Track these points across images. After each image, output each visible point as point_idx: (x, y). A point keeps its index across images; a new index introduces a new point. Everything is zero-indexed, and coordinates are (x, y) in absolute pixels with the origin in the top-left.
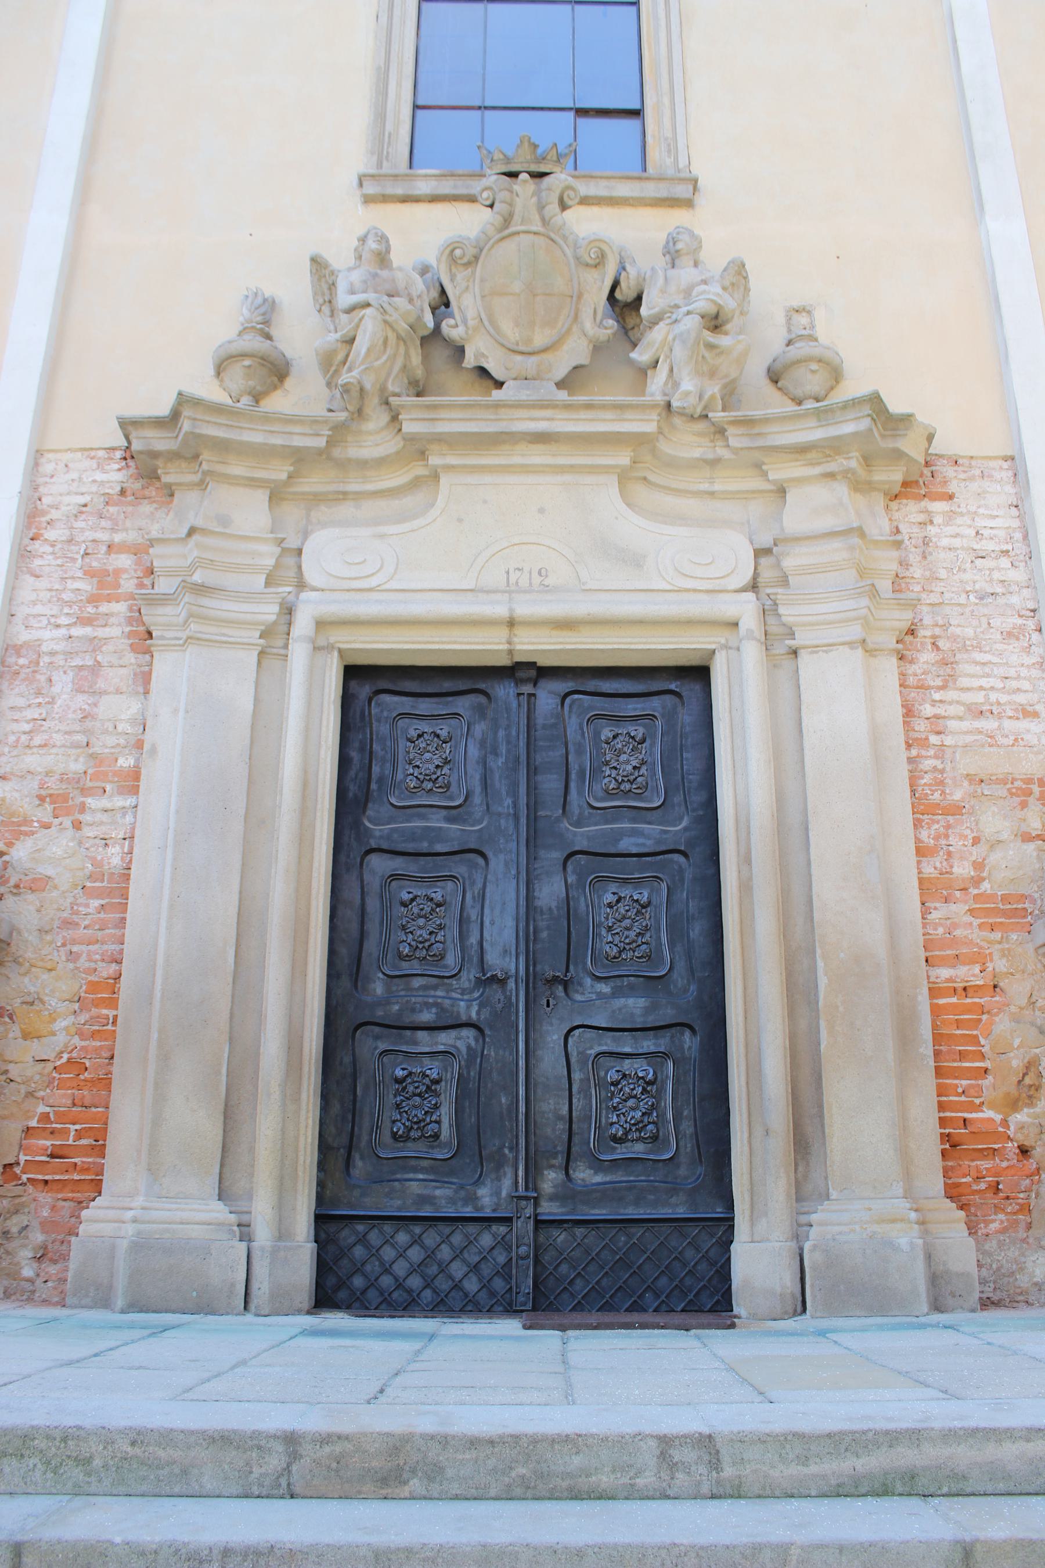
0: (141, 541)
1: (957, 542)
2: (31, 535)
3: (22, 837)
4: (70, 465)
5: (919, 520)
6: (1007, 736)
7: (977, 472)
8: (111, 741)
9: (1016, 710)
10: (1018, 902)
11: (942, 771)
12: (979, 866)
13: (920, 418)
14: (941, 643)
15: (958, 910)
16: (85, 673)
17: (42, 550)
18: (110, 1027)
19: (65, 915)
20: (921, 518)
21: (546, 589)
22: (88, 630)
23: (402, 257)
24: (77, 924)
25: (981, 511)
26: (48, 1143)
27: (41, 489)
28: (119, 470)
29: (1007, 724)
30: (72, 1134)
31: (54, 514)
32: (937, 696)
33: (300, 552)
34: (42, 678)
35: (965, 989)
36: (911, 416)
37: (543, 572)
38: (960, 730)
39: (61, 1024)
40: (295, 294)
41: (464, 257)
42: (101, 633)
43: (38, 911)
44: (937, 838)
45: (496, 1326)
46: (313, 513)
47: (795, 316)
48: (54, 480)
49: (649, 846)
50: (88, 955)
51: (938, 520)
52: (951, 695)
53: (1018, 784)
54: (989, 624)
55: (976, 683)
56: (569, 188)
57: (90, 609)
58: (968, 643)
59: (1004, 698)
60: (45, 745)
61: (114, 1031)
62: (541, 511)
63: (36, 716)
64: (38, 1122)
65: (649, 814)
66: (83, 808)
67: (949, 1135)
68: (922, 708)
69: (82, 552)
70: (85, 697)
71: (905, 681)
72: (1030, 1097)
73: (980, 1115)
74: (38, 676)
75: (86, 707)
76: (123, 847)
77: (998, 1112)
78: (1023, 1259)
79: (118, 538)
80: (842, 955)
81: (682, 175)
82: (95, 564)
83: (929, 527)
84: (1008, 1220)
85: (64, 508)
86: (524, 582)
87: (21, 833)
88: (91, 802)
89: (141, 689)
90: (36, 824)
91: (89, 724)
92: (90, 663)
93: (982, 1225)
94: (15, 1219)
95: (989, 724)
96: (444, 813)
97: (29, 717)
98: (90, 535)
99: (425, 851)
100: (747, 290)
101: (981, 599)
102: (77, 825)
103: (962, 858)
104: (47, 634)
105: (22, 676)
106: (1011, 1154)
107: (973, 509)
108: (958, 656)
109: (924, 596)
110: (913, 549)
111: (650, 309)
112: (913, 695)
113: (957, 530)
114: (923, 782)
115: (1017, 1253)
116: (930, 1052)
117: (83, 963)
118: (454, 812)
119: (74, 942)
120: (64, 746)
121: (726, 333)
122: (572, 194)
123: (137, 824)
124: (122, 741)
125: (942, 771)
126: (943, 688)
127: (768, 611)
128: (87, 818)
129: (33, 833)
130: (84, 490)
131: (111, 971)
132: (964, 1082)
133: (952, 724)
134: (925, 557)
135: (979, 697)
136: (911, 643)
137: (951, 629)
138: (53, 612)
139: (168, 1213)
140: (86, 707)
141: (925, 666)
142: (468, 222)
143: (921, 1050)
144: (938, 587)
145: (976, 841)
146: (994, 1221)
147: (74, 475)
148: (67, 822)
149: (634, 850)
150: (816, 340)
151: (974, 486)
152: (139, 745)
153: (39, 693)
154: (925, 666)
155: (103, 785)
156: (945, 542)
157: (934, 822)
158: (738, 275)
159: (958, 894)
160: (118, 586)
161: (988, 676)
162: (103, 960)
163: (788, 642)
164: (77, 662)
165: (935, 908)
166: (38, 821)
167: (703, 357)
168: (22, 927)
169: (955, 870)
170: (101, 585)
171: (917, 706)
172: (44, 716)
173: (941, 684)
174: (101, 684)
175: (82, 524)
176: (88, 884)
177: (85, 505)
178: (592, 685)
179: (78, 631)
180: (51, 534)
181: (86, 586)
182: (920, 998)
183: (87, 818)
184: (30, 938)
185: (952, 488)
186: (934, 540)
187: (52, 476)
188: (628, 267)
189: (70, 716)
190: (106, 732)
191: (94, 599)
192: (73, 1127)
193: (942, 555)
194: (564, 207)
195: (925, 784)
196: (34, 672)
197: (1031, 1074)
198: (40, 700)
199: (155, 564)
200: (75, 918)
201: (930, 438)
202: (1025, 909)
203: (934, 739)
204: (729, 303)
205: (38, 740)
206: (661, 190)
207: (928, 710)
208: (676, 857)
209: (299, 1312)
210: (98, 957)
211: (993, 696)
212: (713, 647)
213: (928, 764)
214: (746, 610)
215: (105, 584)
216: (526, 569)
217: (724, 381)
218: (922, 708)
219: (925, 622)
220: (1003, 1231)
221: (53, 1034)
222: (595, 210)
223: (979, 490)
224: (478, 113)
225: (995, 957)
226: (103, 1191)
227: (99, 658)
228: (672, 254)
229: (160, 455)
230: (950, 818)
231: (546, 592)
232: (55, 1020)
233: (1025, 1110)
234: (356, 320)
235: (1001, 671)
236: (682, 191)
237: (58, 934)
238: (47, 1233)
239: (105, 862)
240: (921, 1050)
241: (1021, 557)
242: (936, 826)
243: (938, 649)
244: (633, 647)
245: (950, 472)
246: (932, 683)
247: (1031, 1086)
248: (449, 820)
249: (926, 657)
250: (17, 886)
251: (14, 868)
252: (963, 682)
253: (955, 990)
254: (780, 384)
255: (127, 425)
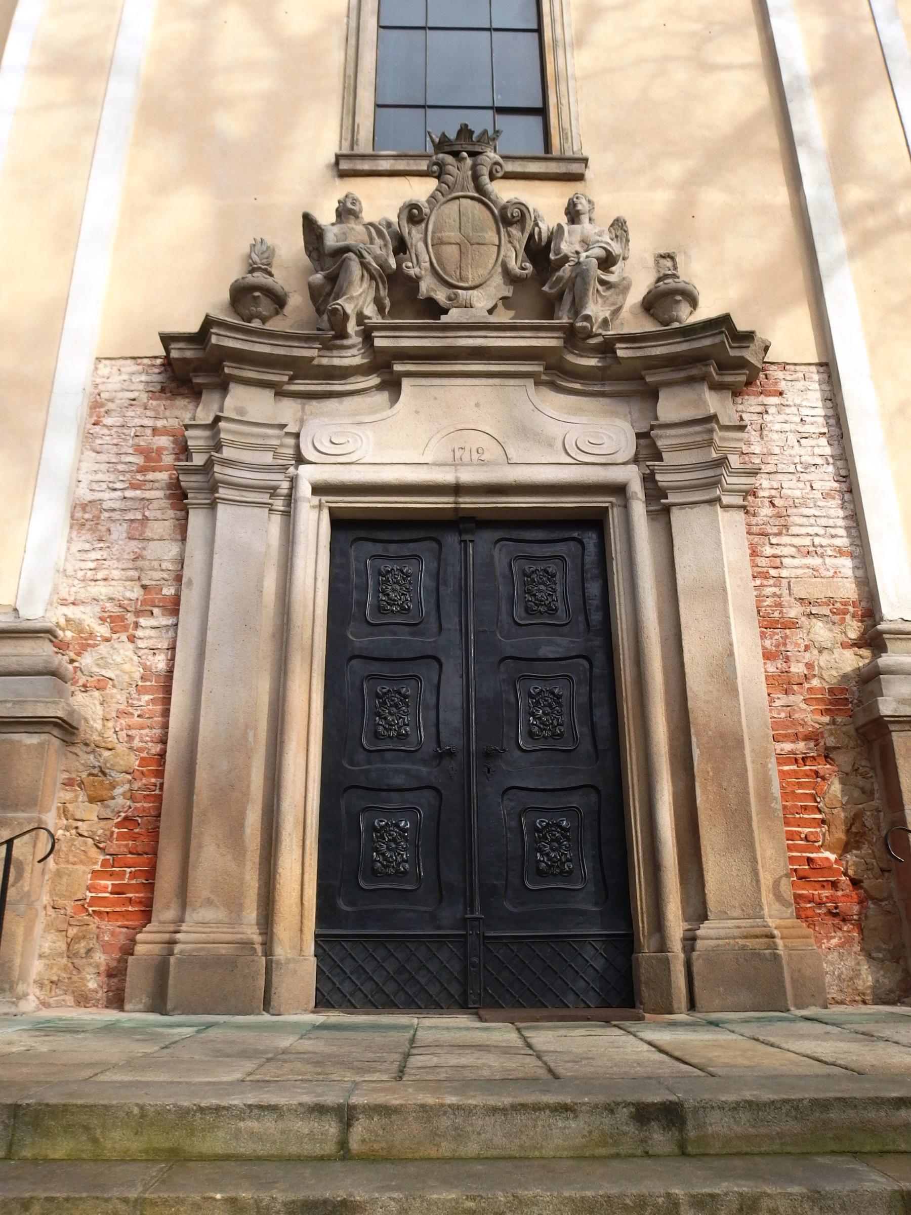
0: (177, 426)
1: (787, 427)
2: (93, 422)
3: (89, 649)
4: (122, 369)
5: (758, 411)
6: (828, 570)
7: (801, 375)
8: (157, 575)
9: (835, 550)
10: (841, 693)
11: (780, 597)
12: (809, 666)
13: (759, 334)
14: (777, 502)
15: (797, 699)
16: (135, 525)
17: (101, 432)
18: (157, 792)
19: (122, 707)
20: (760, 409)
21: (483, 463)
22: (138, 493)
23: (370, 214)
24: (132, 714)
25: (804, 403)
26: (109, 883)
27: (100, 387)
28: (159, 373)
29: (828, 560)
30: (127, 876)
31: (111, 406)
32: (774, 541)
33: (297, 436)
34: (103, 529)
35: (803, 759)
36: (753, 332)
37: (480, 451)
38: (794, 567)
39: (119, 791)
40: (290, 246)
41: (414, 214)
42: (148, 494)
43: (101, 704)
44: (777, 646)
45: (457, 1020)
46: (306, 407)
47: (662, 261)
48: (110, 380)
49: (562, 652)
50: (141, 737)
51: (772, 410)
52: (785, 539)
53: (838, 605)
54: (812, 487)
55: (803, 531)
56: (497, 163)
57: (139, 477)
58: (796, 501)
59: (825, 542)
60: (105, 580)
61: (161, 795)
62: (477, 405)
63: (99, 557)
64: (102, 866)
65: (560, 629)
66: (136, 626)
67: (795, 870)
68: (763, 549)
69: (132, 434)
70: (135, 543)
71: (750, 529)
72: (857, 842)
73: (820, 855)
74: (100, 527)
75: (137, 550)
76: (167, 656)
77: (833, 853)
78: (858, 968)
79: (160, 424)
80: (710, 733)
81: (577, 156)
82: (142, 443)
83: (765, 416)
84: (845, 937)
85: (118, 402)
86: (466, 458)
87: (89, 645)
88: (142, 621)
89: (179, 537)
90: (99, 639)
91: (140, 563)
92: (140, 517)
93: (825, 941)
94: (83, 944)
95: (815, 561)
96: (407, 629)
97: (93, 558)
98: (138, 422)
99: (395, 657)
100: (628, 241)
101: (806, 468)
102: (132, 639)
103: (798, 661)
104: (107, 495)
105: (88, 527)
106: (844, 885)
107: (798, 402)
108: (790, 511)
109: (763, 467)
110: (754, 433)
111: (556, 255)
112: (756, 540)
113: (787, 418)
114: (766, 604)
115: (853, 963)
116: (779, 807)
117: (136, 743)
118: (415, 628)
119: (129, 727)
120: (120, 580)
121: (612, 273)
122: (498, 168)
123: (178, 638)
124: (165, 576)
125: (780, 597)
126: (779, 534)
127: (649, 480)
128: (139, 633)
129: (98, 645)
130: (133, 388)
131: (158, 749)
132: (807, 830)
133: (786, 561)
134: (762, 439)
135: (807, 541)
136: (753, 502)
137: (783, 491)
138: (111, 480)
139: (204, 935)
140: (137, 550)
141: (765, 519)
142: (421, 190)
143: (773, 805)
144: (773, 460)
145: (807, 648)
146: (834, 937)
147: (125, 377)
148: (124, 637)
149: (551, 656)
150: (678, 278)
151: (800, 385)
152: (179, 579)
153: (100, 540)
154: (765, 519)
155: (151, 608)
156: (778, 427)
157: (775, 634)
158: (619, 226)
159: (795, 687)
160: (160, 460)
161: (811, 526)
162: (152, 741)
163: (663, 501)
164: (130, 516)
165: (779, 698)
166: (101, 636)
167: (597, 290)
168: (89, 717)
169: (792, 669)
170: (147, 459)
171: (759, 547)
172: (105, 557)
173: (777, 531)
174: (148, 534)
175: (132, 414)
176: (140, 683)
177: (134, 400)
178: (515, 534)
179: (129, 494)
180: (108, 421)
181: (139, 460)
182: (770, 766)
183: (139, 633)
184: (95, 725)
185: (783, 386)
186: (769, 425)
187: (108, 378)
188: (540, 224)
189: (126, 557)
190: (153, 569)
191: (142, 470)
192: (128, 870)
193: (775, 436)
194: (492, 178)
195: (768, 606)
196: (97, 524)
197: (857, 824)
198: (102, 545)
199: (189, 443)
200: (131, 710)
201: (766, 349)
202: (847, 699)
203: (773, 572)
204: (616, 248)
205: (100, 575)
206: (561, 168)
207: (768, 551)
208: (581, 661)
209: (305, 1011)
210: (148, 739)
211: (817, 540)
212: (607, 505)
213: (769, 591)
214: (632, 476)
215: (151, 457)
216: (467, 449)
217: (613, 308)
218: (763, 549)
219: (763, 486)
220: (841, 945)
221: (113, 798)
222: (512, 183)
223: (803, 388)
224: (422, 111)
225: (826, 735)
226: (152, 919)
227: (147, 514)
228: (573, 214)
229: (192, 367)
230: (787, 631)
231: (482, 465)
232: (114, 787)
233: (855, 852)
234: (339, 263)
235: (823, 522)
236: (575, 168)
237: (116, 721)
238: (107, 953)
239: (153, 667)
240: (773, 805)
241: (835, 438)
242: (776, 637)
243: (774, 505)
244: (547, 505)
245: (780, 374)
246: (770, 531)
247: (857, 833)
248: (413, 634)
249: (766, 511)
250: (84, 686)
251: (82, 672)
252: (794, 530)
253: (796, 760)
254: (652, 311)
255: (167, 339)
